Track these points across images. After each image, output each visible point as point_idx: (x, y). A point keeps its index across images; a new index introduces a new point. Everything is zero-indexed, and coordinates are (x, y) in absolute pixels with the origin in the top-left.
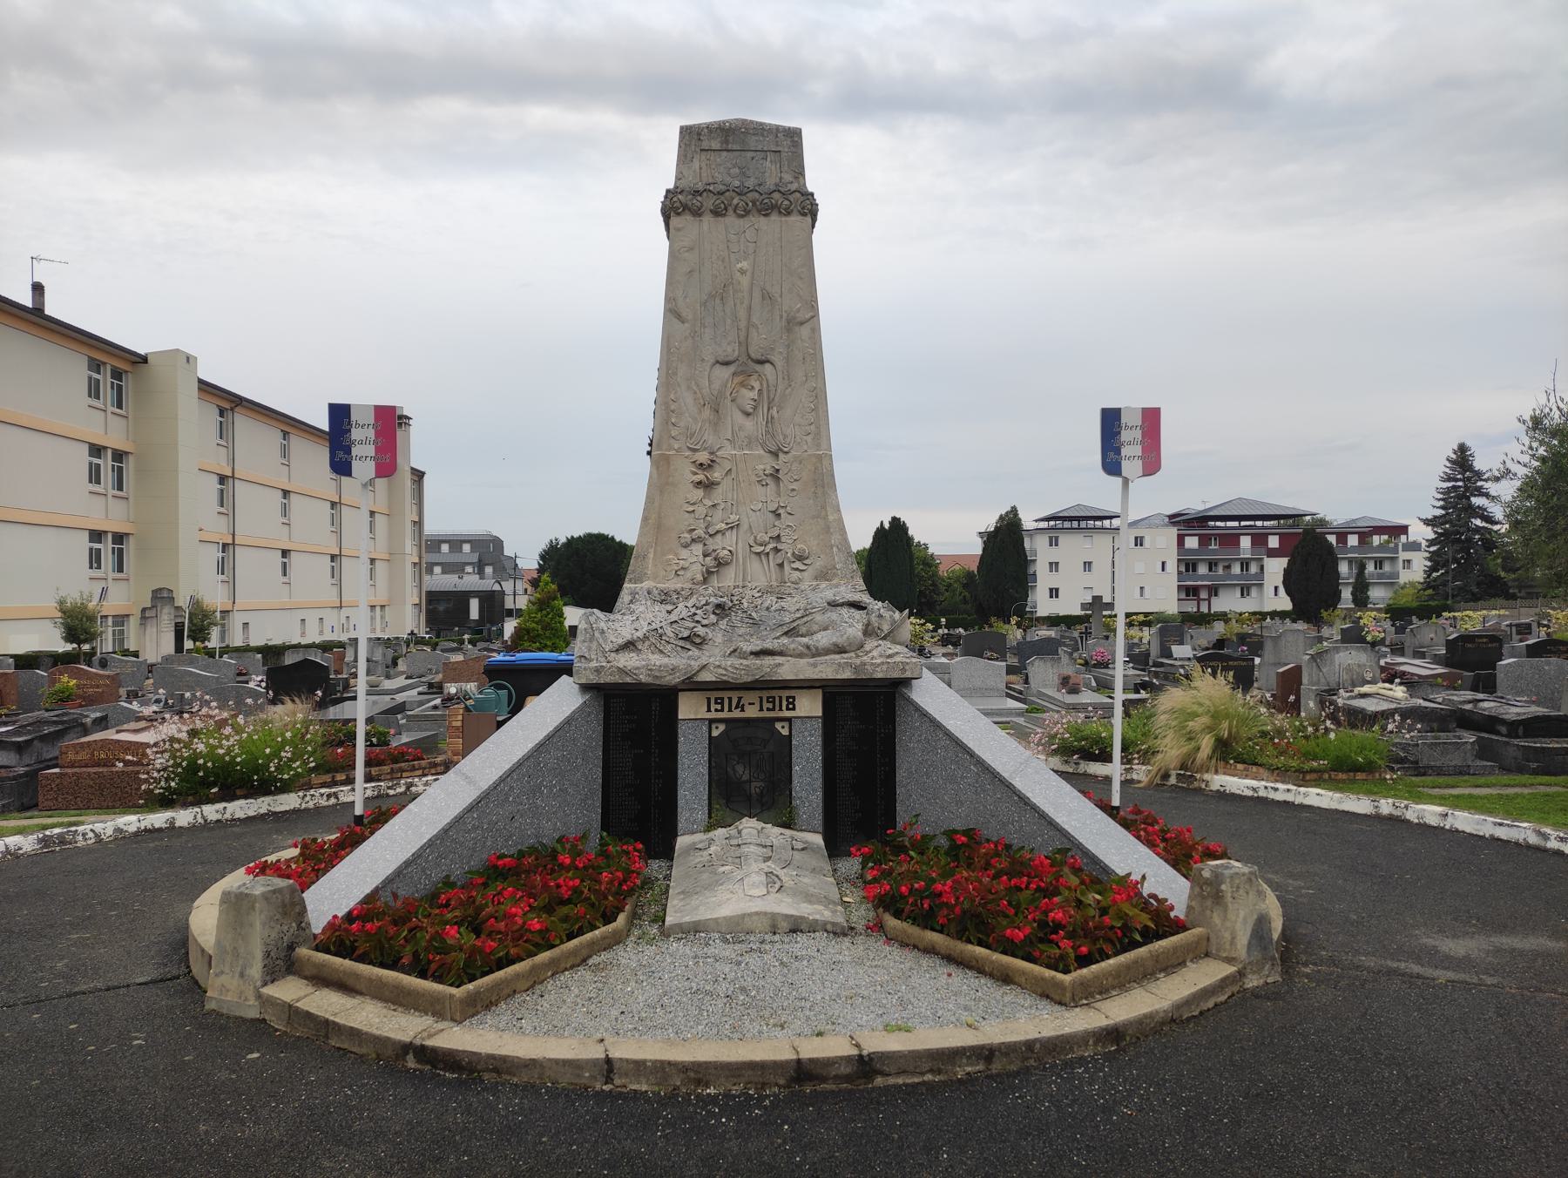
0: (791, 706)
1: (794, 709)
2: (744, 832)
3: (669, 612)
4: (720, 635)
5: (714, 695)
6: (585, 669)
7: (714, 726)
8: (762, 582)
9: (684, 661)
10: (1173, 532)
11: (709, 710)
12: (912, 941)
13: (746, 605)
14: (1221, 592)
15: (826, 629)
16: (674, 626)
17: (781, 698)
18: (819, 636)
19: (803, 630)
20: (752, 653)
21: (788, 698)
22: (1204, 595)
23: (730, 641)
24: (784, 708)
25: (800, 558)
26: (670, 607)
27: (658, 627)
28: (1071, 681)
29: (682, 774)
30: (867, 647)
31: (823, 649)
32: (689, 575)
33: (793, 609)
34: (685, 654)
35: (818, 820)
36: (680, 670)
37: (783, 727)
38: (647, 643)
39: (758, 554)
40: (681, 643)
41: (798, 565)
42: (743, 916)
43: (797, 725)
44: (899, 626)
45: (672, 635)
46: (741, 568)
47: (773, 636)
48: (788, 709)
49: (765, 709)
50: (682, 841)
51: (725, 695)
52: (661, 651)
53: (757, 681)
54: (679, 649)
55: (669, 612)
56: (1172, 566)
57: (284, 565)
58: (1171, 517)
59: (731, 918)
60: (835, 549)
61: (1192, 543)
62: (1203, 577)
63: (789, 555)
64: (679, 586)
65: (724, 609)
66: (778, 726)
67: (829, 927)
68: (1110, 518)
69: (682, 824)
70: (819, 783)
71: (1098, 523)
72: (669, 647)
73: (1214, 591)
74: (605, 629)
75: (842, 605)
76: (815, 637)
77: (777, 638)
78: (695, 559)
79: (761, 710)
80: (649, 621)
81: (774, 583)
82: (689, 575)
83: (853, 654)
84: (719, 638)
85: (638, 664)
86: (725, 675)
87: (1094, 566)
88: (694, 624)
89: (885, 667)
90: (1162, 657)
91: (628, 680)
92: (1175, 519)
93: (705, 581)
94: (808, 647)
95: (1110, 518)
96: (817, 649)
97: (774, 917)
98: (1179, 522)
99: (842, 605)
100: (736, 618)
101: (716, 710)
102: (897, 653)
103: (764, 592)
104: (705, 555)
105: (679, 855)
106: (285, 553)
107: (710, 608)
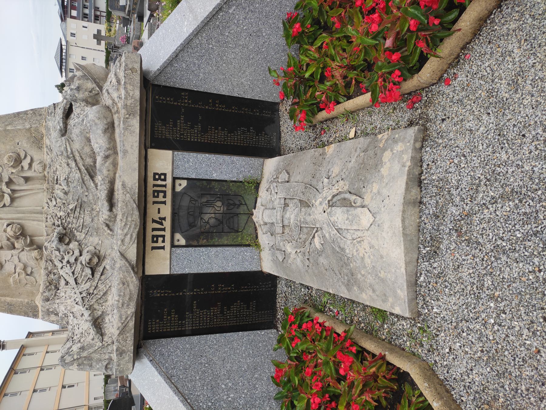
0: (163, 177)
1: (165, 175)
2: (266, 220)
3: (67, 283)
4: (91, 239)
5: (149, 244)
6: (118, 366)
7: (176, 243)
8: (43, 197)
9: (116, 273)
10: (69, 20)
11: (163, 248)
12: (458, 50)
13: (62, 213)
14: (98, 6)
15: (89, 140)
16: (79, 281)
17: (155, 186)
18: (96, 146)
19: (89, 161)
20: (111, 210)
21: (155, 179)
22: (98, 13)
23: (97, 230)
24: (163, 183)
25: (18, 161)
26: (63, 282)
27: (80, 296)
28: (136, 46)
29: (216, 269)
30: (109, 102)
31: (110, 143)
32: (32, 263)
33: (67, 170)
34: (109, 272)
35: (255, 161)
36: (125, 277)
37: (180, 185)
38: (96, 306)
39: (13, 200)
40: (97, 275)
41: (25, 164)
42: (405, 235)
43: (178, 174)
44: (89, 72)
45: (88, 284)
46: (28, 215)
47: (94, 190)
48: (165, 180)
49: (163, 200)
50: (268, 267)
51: (150, 234)
52: (105, 294)
53: (139, 206)
54: (103, 277)
55: (67, 283)
56: (85, 24)
57: (69, 387)
58: (62, 20)
59: (406, 248)
60: (9, 128)
61: (74, 13)
62: (90, 12)
63: (14, 171)
64: (43, 272)
65: (65, 235)
66: (178, 189)
67: (418, 145)
68: (61, 45)
69: (254, 268)
70: (227, 158)
71: (64, 51)
72: (101, 286)
73: (97, 9)
74: (79, 345)
75: (66, 124)
76: (97, 150)
77: (96, 186)
78: (16, 259)
79: (164, 203)
80: (74, 303)
81: (45, 186)
82: (32, 263)
83: (115, 117)
84: (93, 240)
85: (116, 317)
86: (132, 235)
87: (84, 56)
88: (78, 263)
89: (129, 87)
90: (125, 11)
91: (132, 324)
92: (63, 18)
93: (40, 248)
94: (107, 157)
95: (61, 45)
96: (109, 149)
97: (407, 203)
98: (64, 17)
99: (66, 124)
100: (74, 224)
101: (163, 241)
102: (115, 75)
103: (52, 197)
104: (14, 248)
105: (287, 275)
106: (64, 387)
107: (63, 248)
